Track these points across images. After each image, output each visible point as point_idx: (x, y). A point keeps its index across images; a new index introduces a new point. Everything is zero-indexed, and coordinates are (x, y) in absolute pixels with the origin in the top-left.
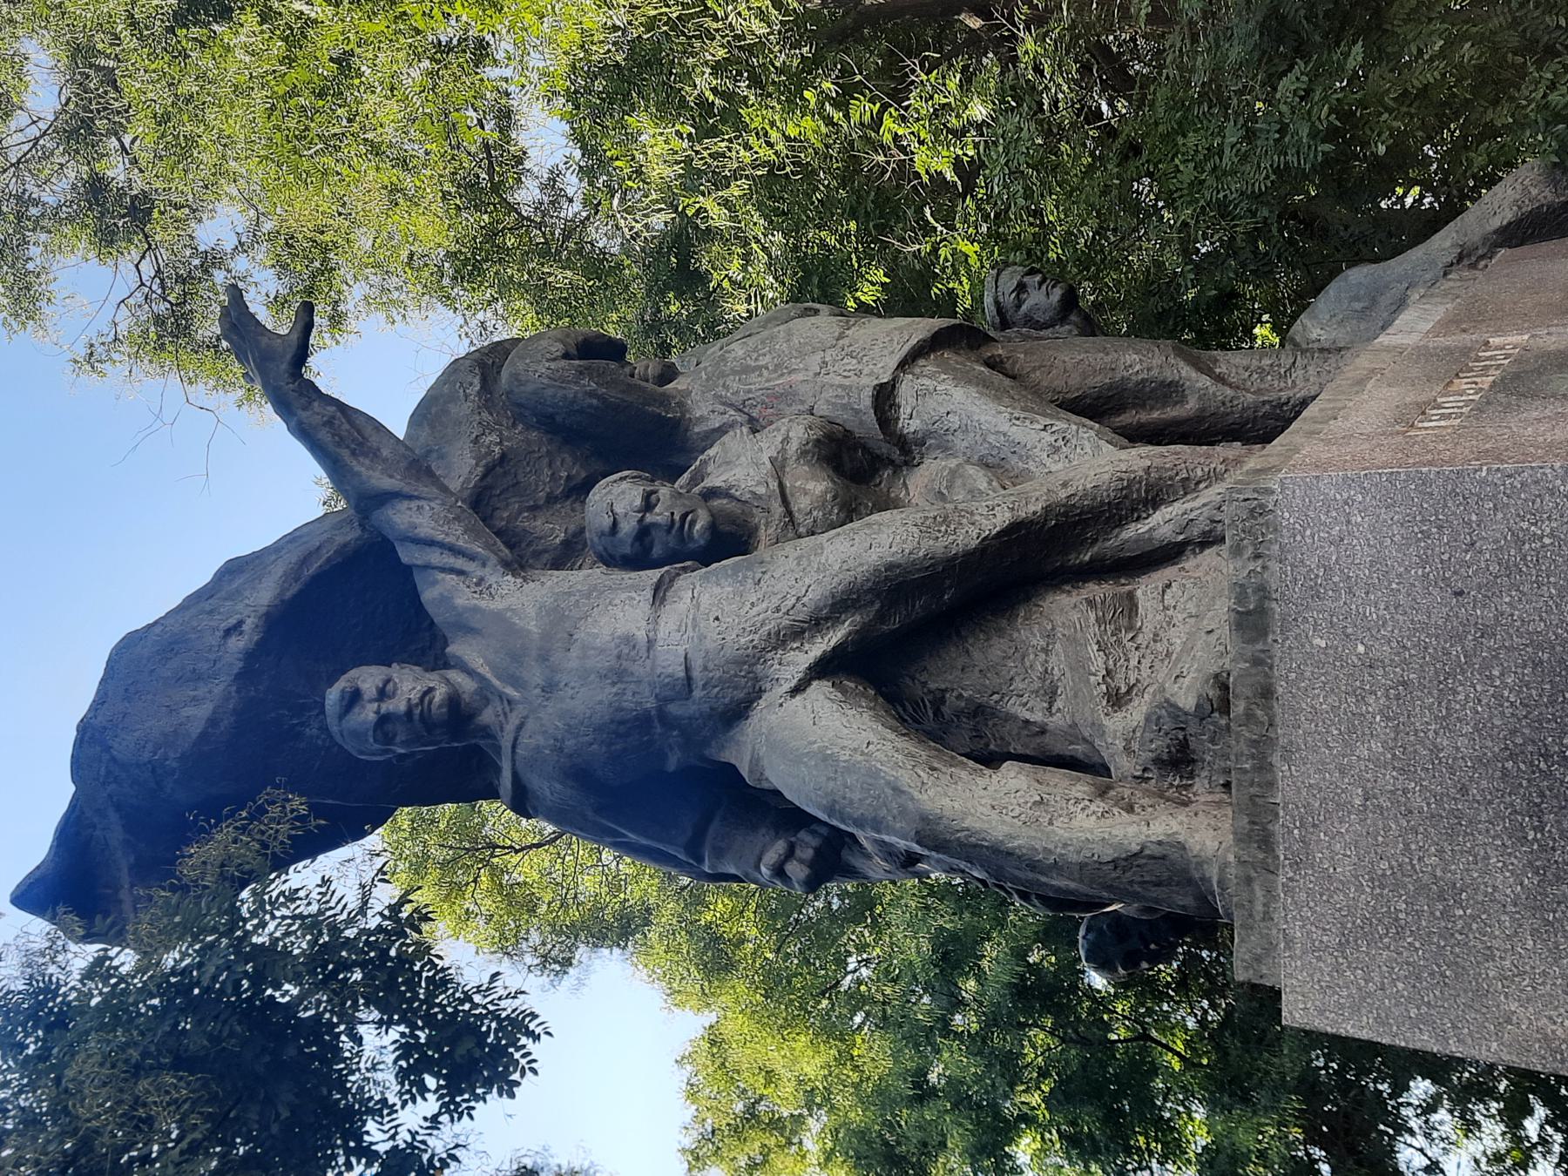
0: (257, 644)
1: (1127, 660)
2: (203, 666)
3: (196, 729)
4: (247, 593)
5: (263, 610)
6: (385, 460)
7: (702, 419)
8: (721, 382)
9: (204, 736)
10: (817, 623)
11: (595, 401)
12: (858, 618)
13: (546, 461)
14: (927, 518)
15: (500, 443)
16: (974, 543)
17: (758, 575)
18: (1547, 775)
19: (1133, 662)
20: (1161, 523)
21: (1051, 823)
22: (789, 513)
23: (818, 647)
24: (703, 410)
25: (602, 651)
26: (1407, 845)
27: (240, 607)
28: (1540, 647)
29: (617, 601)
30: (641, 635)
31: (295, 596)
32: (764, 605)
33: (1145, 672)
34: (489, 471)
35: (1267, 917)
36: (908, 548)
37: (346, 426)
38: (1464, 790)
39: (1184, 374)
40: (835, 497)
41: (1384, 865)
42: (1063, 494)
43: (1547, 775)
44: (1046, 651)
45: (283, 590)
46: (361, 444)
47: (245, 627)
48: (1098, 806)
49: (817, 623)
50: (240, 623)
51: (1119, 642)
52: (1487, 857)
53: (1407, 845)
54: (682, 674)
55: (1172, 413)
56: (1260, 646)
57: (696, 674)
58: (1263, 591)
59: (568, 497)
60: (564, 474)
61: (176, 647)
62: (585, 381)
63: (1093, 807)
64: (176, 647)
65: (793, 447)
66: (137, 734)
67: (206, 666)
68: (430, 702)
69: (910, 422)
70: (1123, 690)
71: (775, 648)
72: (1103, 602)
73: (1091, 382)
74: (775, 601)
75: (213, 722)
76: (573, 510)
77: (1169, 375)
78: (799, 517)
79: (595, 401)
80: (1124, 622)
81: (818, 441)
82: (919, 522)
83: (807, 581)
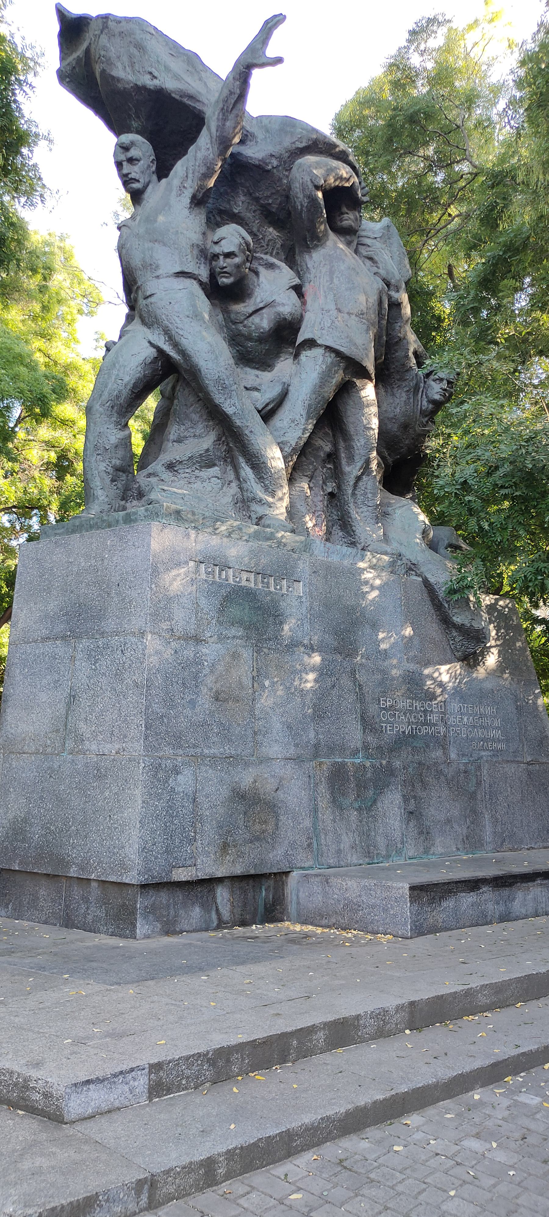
0: (150, 89)
1: (187, 468)
2: (137, 67)
3: (114, 73)
4: (170, 75)
5: (164, 87)
6: (224, 125)
7: (311, 257)
8: (327, 263)
9: (113, 77)
10: (176, 345)
11: (299, 207)
12: (182, 361)
13: (274, 191)
14: (224, 380)
15: (273, 168)
16: (217, 402)
17: (191, 316)
18: (75, 616)
19: (187, 471)
20: (247, 471)
21: (98, 455)
22: (251, 315)
23: (167, 348)
24: (315, 260)
25: (151, 257)
26: (60, 576)
27: (163, 74)
28: (104, 611)
29: (174, 257)
30: (160, 272)
31: (174, 98)
32: (179, 322)
33: (183, 475)
34: (258, 167)
35: (56, 534)
36: (209, 376)
37: (233, 101)
38: (72, 592)
39: (358, 464)
40: (262, 333)
41: (56, 570)
42: (247, 432)
43: (75, 616)
44: (195, 436)
45: (174, 92)
46: (227, 111)
47: (155, 80)
48: (110, 469)
49: (176, 345)
50: (156, 78)
51: (194, 464)
52: (57, 600)
53: (60, 576)
54: (148, 295)
55: (344, 462)
56: (122, 522)
57: (149, 300)
58: (135, 521)
59: (261, 206)
60: (270, 201)
61: (141, 51)
62: (306, 201)
63: (109, 468)
64: (141, 51)
65: (281, 309)
66: (108, 45)
67: (137, 68)
68: (132, 183)
69: (306, 356)
70: (175, 469)
71: (164, 330)
72: (209, 455)
73: (351, 426)
74: (180, 326)
75: (119, 80)
76: (254, 212)
77: (357, 458)
78: (251, 319)
79: (299, 207)
80: (203, 464)
81: (286, 319)
82: (221, 378)
83: (190, 337)
